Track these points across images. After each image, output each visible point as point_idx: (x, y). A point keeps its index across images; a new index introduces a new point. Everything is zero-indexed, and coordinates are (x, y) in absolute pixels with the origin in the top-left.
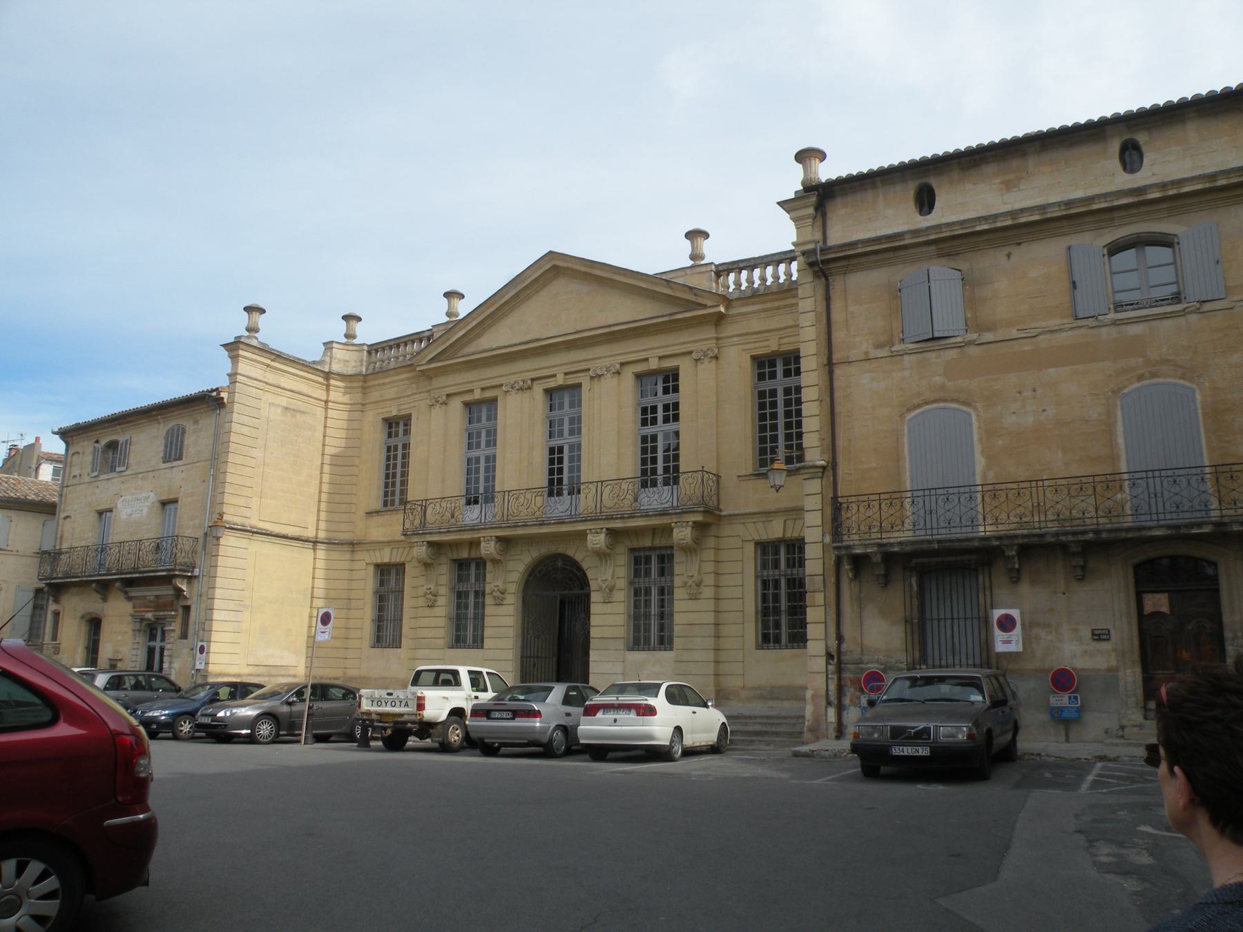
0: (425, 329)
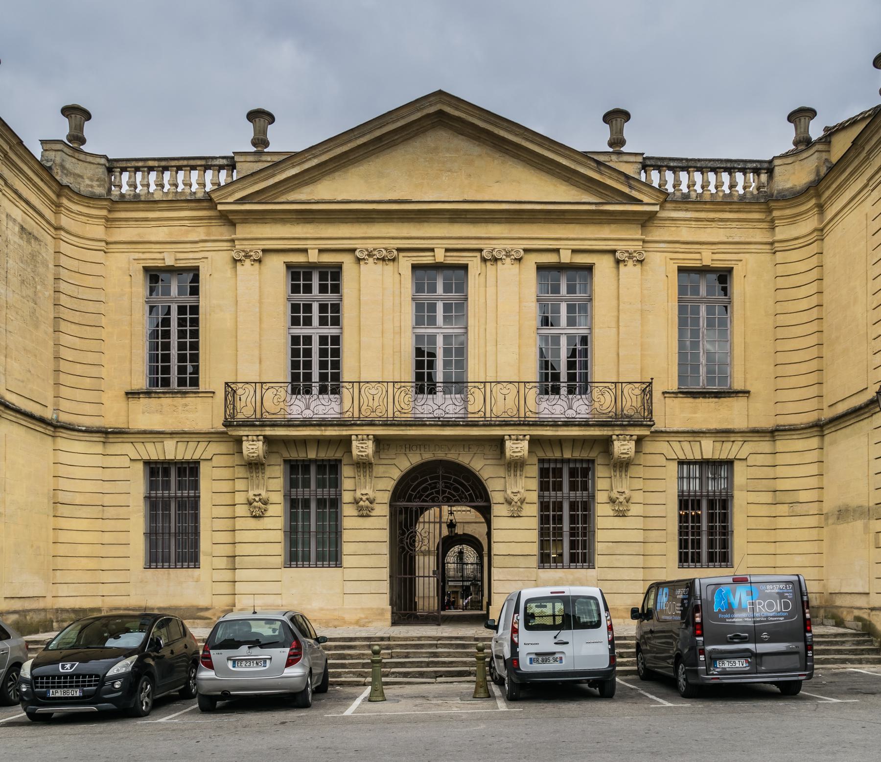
0: (218, 156)
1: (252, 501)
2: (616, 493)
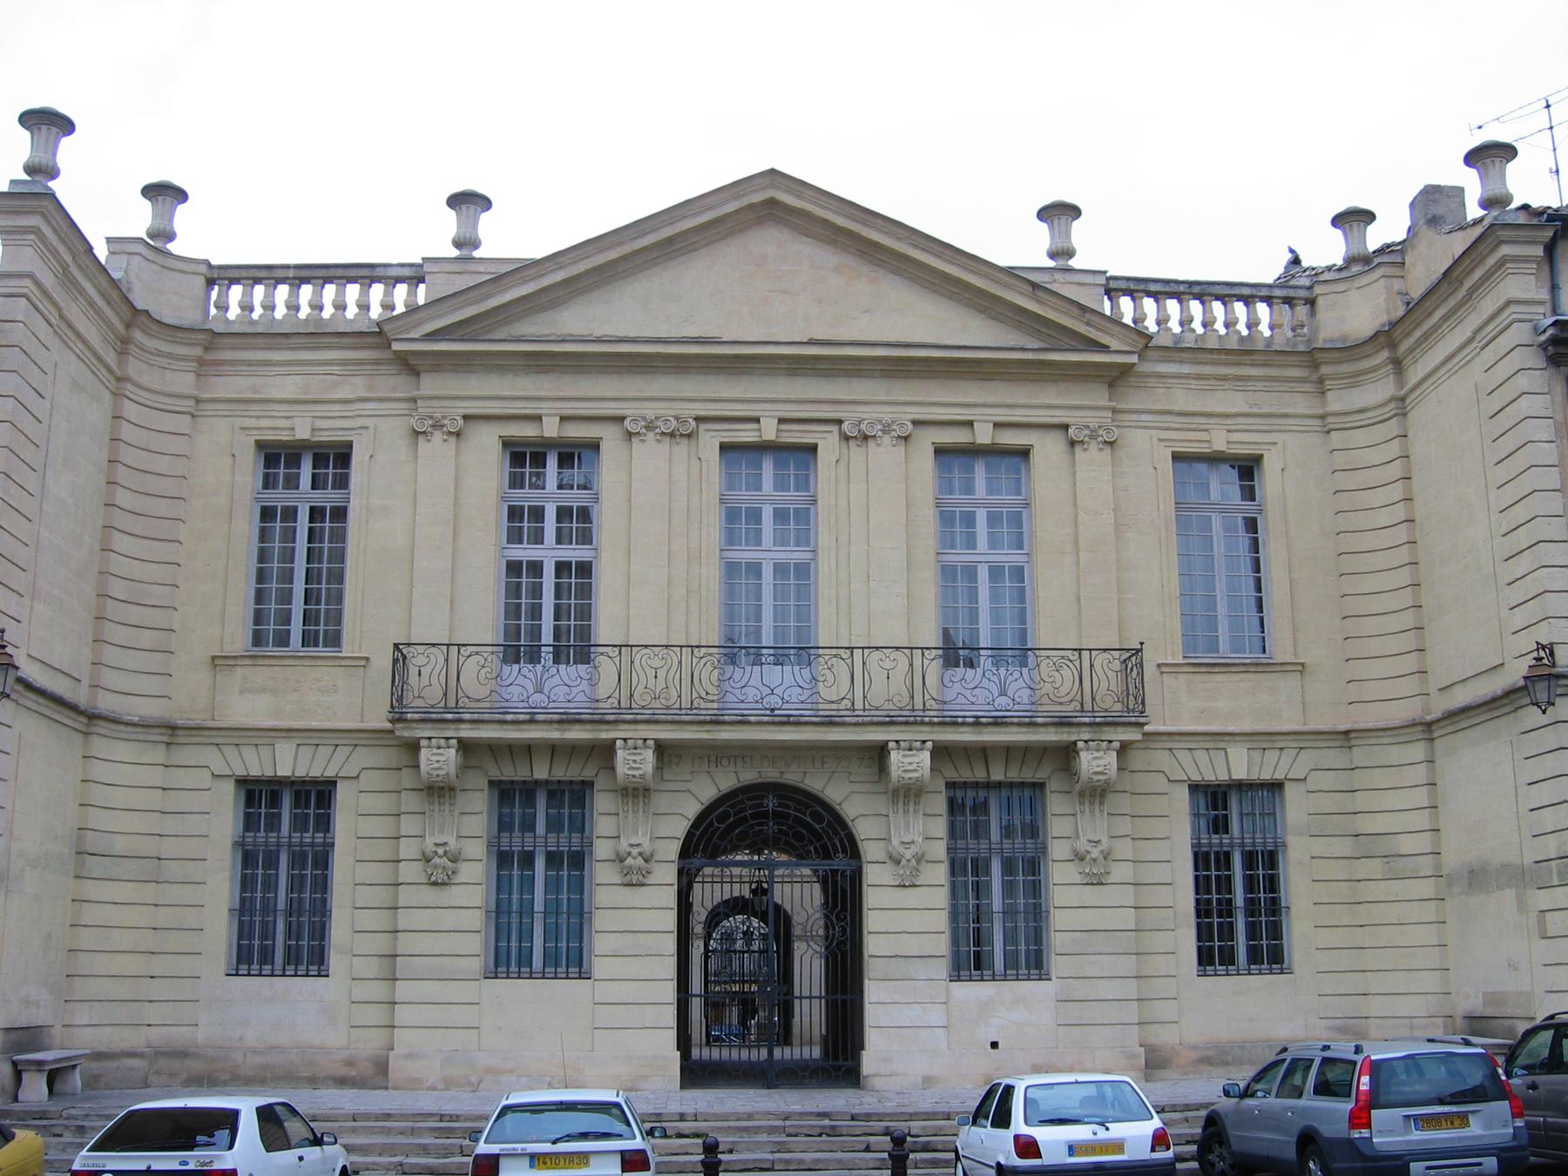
1: (432, 854)
2: (1086, 842)
